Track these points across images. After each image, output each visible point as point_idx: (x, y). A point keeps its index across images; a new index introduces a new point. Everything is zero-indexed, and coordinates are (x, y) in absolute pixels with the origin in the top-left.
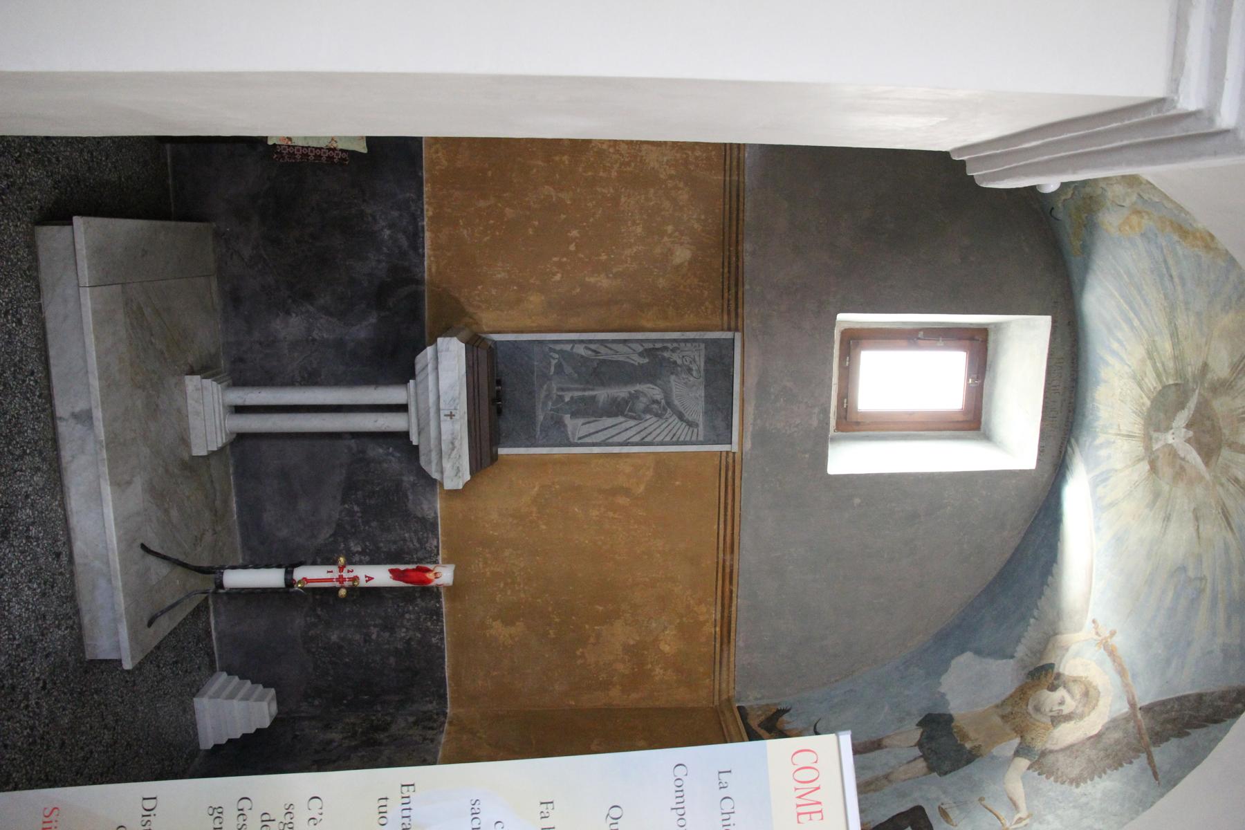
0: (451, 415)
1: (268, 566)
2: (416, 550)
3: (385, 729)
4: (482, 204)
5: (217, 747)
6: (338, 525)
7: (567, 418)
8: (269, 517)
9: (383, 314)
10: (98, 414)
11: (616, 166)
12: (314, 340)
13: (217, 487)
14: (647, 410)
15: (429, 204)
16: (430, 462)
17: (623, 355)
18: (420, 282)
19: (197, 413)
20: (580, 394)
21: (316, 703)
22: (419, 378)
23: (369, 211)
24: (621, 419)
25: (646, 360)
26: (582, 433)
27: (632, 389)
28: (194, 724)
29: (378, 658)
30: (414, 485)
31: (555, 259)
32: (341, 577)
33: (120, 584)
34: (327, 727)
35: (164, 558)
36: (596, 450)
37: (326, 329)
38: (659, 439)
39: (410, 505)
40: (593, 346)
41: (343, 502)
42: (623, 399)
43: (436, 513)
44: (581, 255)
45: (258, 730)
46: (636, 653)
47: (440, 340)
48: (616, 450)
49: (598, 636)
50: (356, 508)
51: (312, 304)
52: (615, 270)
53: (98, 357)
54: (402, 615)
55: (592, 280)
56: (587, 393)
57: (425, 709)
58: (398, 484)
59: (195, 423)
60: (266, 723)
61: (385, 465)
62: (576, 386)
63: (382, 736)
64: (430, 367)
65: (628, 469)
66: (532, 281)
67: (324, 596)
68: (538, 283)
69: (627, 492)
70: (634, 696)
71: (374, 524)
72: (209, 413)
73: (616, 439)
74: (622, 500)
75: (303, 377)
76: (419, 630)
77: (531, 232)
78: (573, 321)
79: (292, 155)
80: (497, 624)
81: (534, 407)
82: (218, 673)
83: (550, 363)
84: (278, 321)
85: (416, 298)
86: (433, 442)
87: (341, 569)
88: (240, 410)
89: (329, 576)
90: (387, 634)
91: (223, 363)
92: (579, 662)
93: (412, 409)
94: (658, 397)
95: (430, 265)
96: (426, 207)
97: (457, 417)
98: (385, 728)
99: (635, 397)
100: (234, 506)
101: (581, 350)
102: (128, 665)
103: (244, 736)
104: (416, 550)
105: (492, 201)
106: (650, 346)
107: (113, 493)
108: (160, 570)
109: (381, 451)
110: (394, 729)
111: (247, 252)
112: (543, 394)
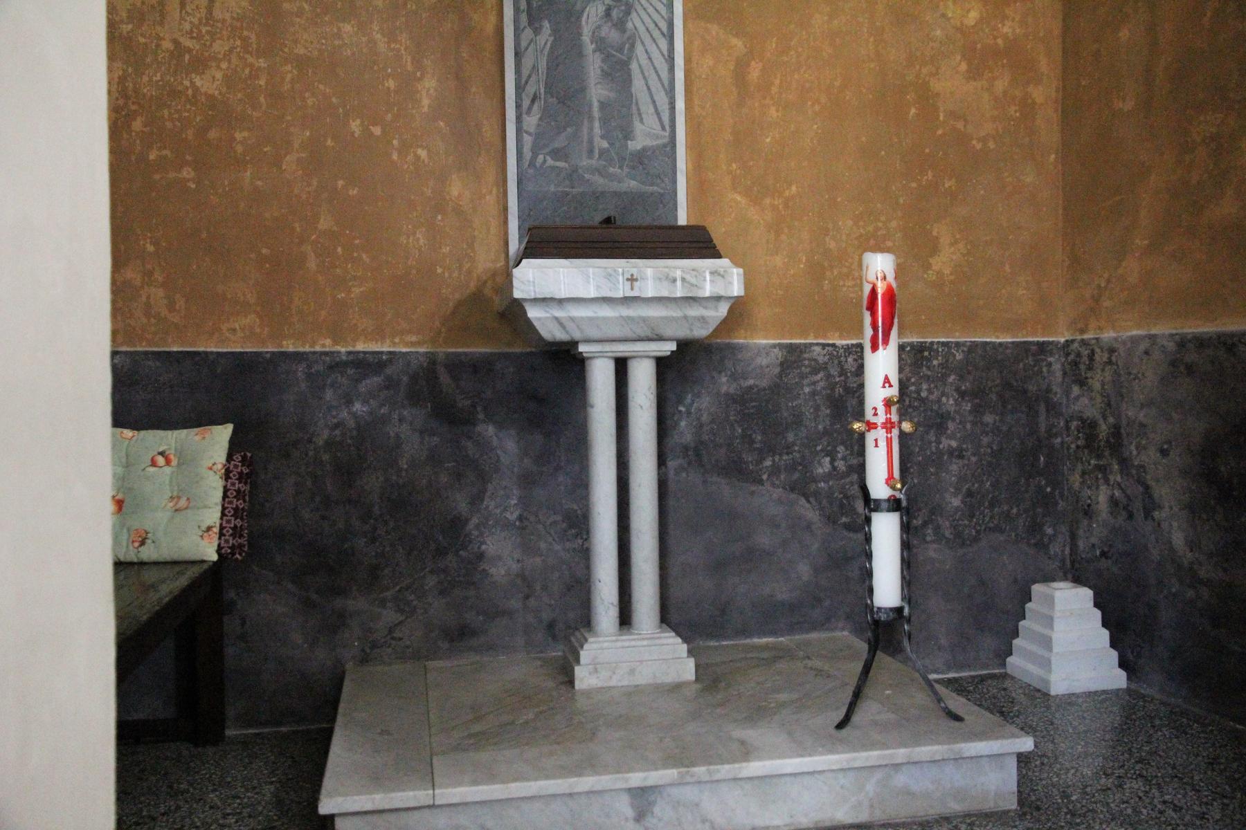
0: (632, 280)
1: (868, 539)
2: (829, 376)
3: (1093, 425)
4: (312, 264)
5: (1123, 664)
6: (792, 490)
7: (635, 145)
8: (782, 592)
9: (481, 416)
10: (637, 779)
11: (250, 59)
12: (520, 518)
14: (620, 25)
15: (313, 344)
16: (702, 319)
17: (537, 59)
18: (432, 359)
19: (632, 672)
21: (1050, 531)
22: (577, 335)
23: (326, 434)
24: (634, 66)
25: (546, 24)
26: (657, 126)
27: (589, 48)
28: (1090, 695)
29: (985, 440)
30: (734, 377)
31: (395, 157)
32: (884, 426)
33: (902, 751)
34: (1088, 512)
35: (857, 695)
36: (680, 105)
37: (504, 501)
38: (664, 11)
39: (764, 383)
40: (526, 103)
41: (761, 482)
42: (603, 61)
43: (774, 346)
45: (1096, 605)
46: (980, 60)
47: (517, 294)
48: (680, 75)
49: (952, 115)
50: (768, 463)
51: (467, 520)
52: (410, 68)
53: (547, 777)
54: (923, 400)
55: (426, 102)
57: (1059, 374)
58: (732, 399)
59: (644, 677)
60: (1086, 594)
61: (705, 418)
62: (585, 131)
63: (1103, 429)
64: (559, 313)
65: (708, 61)
66: (428, 192)
67: (909, 459)
68: (431, 183)
69: (741, 68)
70: (1043, 65)
71: (791, 437)
72: (630, 656)
73: (664, 75)
74: (755, 72)
76: (944, 377)
77: (354, 192)
78: (489, 131)
79: (236, 532)
80: (937, 263)
81: (616, 194)
82: (1009, 671)
83: (553, 168)
84: (493, 571)
85: (456, 365)
87: (871, 426)
88: (625, 619)
89: (883, 444)
90: (951, 426)
91: (556, 652)
92: (991, 145)
93: (622, 349)
94: (602, 9)
95: (405, 343)
96: (318, 349)
97: (634, 271)
98: (1089, 426)
99: (601, 45)
100: (765, 640)
101: (531, 122)
102: (1026, 744)
103: (1105, 624)
104: (829, 376)
105: (307, 248)
106: (524, 18)
107: (760, 759)
108: (868, 711)
109: (683, 424)
110: (1091, 412)
111: (389, 616)
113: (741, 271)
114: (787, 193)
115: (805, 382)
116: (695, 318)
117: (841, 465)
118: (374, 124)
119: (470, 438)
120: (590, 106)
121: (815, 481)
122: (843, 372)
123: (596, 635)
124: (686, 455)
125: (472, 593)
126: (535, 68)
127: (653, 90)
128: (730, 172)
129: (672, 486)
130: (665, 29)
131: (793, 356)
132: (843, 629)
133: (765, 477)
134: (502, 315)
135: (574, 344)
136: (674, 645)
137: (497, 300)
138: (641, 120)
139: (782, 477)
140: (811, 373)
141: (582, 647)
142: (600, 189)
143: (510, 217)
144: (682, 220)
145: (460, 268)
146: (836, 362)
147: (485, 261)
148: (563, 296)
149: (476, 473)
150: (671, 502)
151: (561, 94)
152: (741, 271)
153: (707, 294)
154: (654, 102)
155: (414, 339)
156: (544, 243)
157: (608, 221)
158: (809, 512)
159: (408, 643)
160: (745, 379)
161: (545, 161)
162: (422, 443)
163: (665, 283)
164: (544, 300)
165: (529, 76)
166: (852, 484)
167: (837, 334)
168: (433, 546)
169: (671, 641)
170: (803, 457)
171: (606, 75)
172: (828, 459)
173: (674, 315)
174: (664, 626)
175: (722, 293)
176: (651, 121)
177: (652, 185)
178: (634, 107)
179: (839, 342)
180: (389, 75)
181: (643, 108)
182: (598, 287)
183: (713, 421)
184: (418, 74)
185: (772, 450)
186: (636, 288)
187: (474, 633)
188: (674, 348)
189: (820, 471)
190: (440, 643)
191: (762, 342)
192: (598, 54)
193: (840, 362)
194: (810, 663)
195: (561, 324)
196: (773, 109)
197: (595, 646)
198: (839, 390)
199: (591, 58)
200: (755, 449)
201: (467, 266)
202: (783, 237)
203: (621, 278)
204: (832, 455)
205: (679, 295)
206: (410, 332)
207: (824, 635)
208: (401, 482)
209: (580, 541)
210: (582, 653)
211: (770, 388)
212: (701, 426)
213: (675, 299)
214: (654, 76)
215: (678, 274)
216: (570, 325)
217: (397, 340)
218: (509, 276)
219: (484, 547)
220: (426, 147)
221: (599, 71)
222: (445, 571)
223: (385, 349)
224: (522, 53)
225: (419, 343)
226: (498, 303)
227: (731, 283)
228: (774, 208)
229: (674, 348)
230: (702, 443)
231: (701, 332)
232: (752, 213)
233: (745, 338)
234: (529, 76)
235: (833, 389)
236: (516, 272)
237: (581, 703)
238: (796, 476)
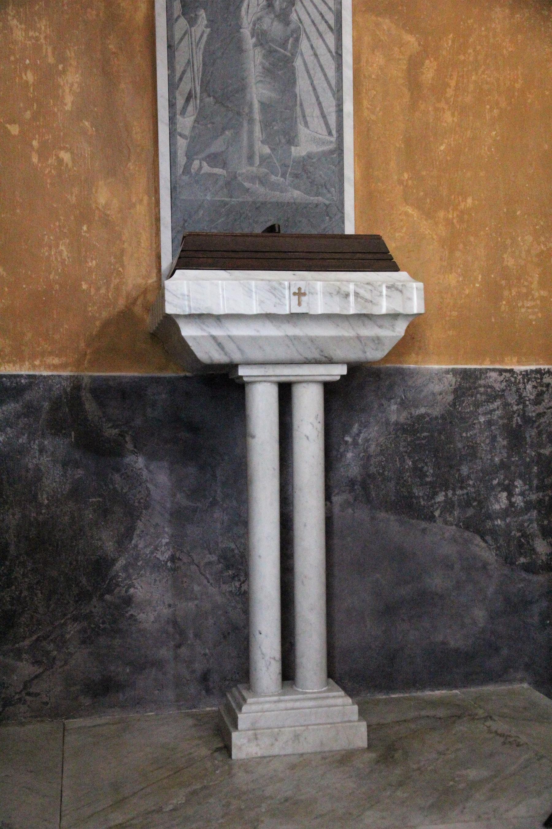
0: (300, 294)
2: (506, 405)
6: (467, 528)
7: (298, 151)
8: (455, 639)
9: (130, 446)
12: (173, 558)
13: (412, 714)
14: (284, 17)
16: (377, 340)
17: (192, 52)
18: (76, 384)
19: (297, 737)
20: (257, 128)
22: (237, 357)
24: (298, 63)
25: (202, 13)
27: (250, 41)
30: (403, 404)
36: (348, 107)
37: (154, 538)
39: (436, 412)
40: (180, 102)
41: (431, 518)
42: (265, 56)
43: (447, 372)
44: (28, 115)
47: (170, 309)
50: (440, 498)
52: (51, 60)
55: (69, 99)
56: (257, 116)
64: (217, 332)
68: (76, 190)
69: (414, 65)
71: (465, 470)
73: (331, 73)
74: (428, 73)
75: (233, 577)
78: (139, 132)
81: (279, 205)
83: (210, 175)
84: (141, 616)
85: (102, 390)
86: (345, 331)
88: (288, 673)
91: (210, 707)
93: (287, 373)
95: (47, 367)
97: (302, 284)
99: (262, 38)
101: (186, 123)
104: (506, 405)
109: (349, 455)
111: (26, 668)
112: (257, 187)
113: (421, 285)
114: (462, 206)
115: (480, 410)
116: (367, 338)
117: (518, 500)
118: (12, 122)
119: (118, 470)
120: (251, 106)
121: (489, 517)
122: (521, 400)
123: (255, 694)
124: (352, 490)
125: (117, 642)
126: (189, 63)
127: (319, 90)
128: (400, 182)
129: (337, 523)
130: (332, 22)
131: (468, 381)
132: (521, 681)
133: (437, 514)
134: (154, 335)
135: (234, 366)
136: (342, 705)
137: (148, 319)
138: (306, 124)
139: (456, 513)
140: (487, 401)
141: (240, 709)
142: (261, 199)
143: (162, 228)
144: (350, 229)
145: (108, 284)
146: (514, 389)
147: (135, 276)
148: (222, 312)
149: (126, 511)
150: (336, 541)
151: (218, 94)
152: (421, 285)
153: (384, 311)
154: (320, 104)
155: (56, 361)
156: (198, 253)
157: (272, 229)
158: (483, 551)
159: (46, 699)
160: (417, 407)
161: (201, 168)
162: (64, 475)
163: (337, 299)
164: (200, 316)
165: (184, 72)
166: (531, 521)
167: (515, 360)
168: (76, 591)
169: (339, 701)
170: (478, 493)
171: (269, 72)
172: (505, 494)
173: (346, 334)
174: (330, 680)
175: (401, 311)
176: (316, 123)
177: (317, 194)
178: (298, 108)
179: (518, 368)
180: (26, 67)
181: (308, 111)
182: (261, 302)
183: (382, 453)
184: (60, 67)
185: (445, 486)
186: (304, 304)
187: (120, 687)
188: (345, 372)
189: (497, 507)
190: (82, 698)
191: (435, 367)
192: (258, 49)
193: (518, 390)
194: (494, 726)
195: (220, 345)
196: (448, 114)
197: (254, 708)
198: (517, 420)
199: (251, 53)
200: (427, 483)
201: (116, 281)
202: (458, 254)
203: (287, 292)
204: (509, 490)
205: (352, 311)
206: (51, 353)
207: (503, 688)
208: (40, 518)
209: (237, 584)
210: (239, 716)
211: (443, 417)
212: (369, 457)
213: (347, 317)
214: (320, 75)
215: (351, 288)
216: (230, 347)
217: (37, 363)
218: (160, 289)
219: (132, 590)
220: (69, 150)
221: (260, 68)
222: (89, 617)
223: (24, 372)
224: (176, 49)
225: (63, 366)
226: (150, 322)
227: (410, 299)
228: (449, 223)
229: (345, 372)
230: (369, 476)
231: (374, 354)
232: (425, 227)
233: (416, 363)
234: (184, 72)
235: (510, 419)
236: (168, 284)
237: (241, 779)
238: (470, 512)
